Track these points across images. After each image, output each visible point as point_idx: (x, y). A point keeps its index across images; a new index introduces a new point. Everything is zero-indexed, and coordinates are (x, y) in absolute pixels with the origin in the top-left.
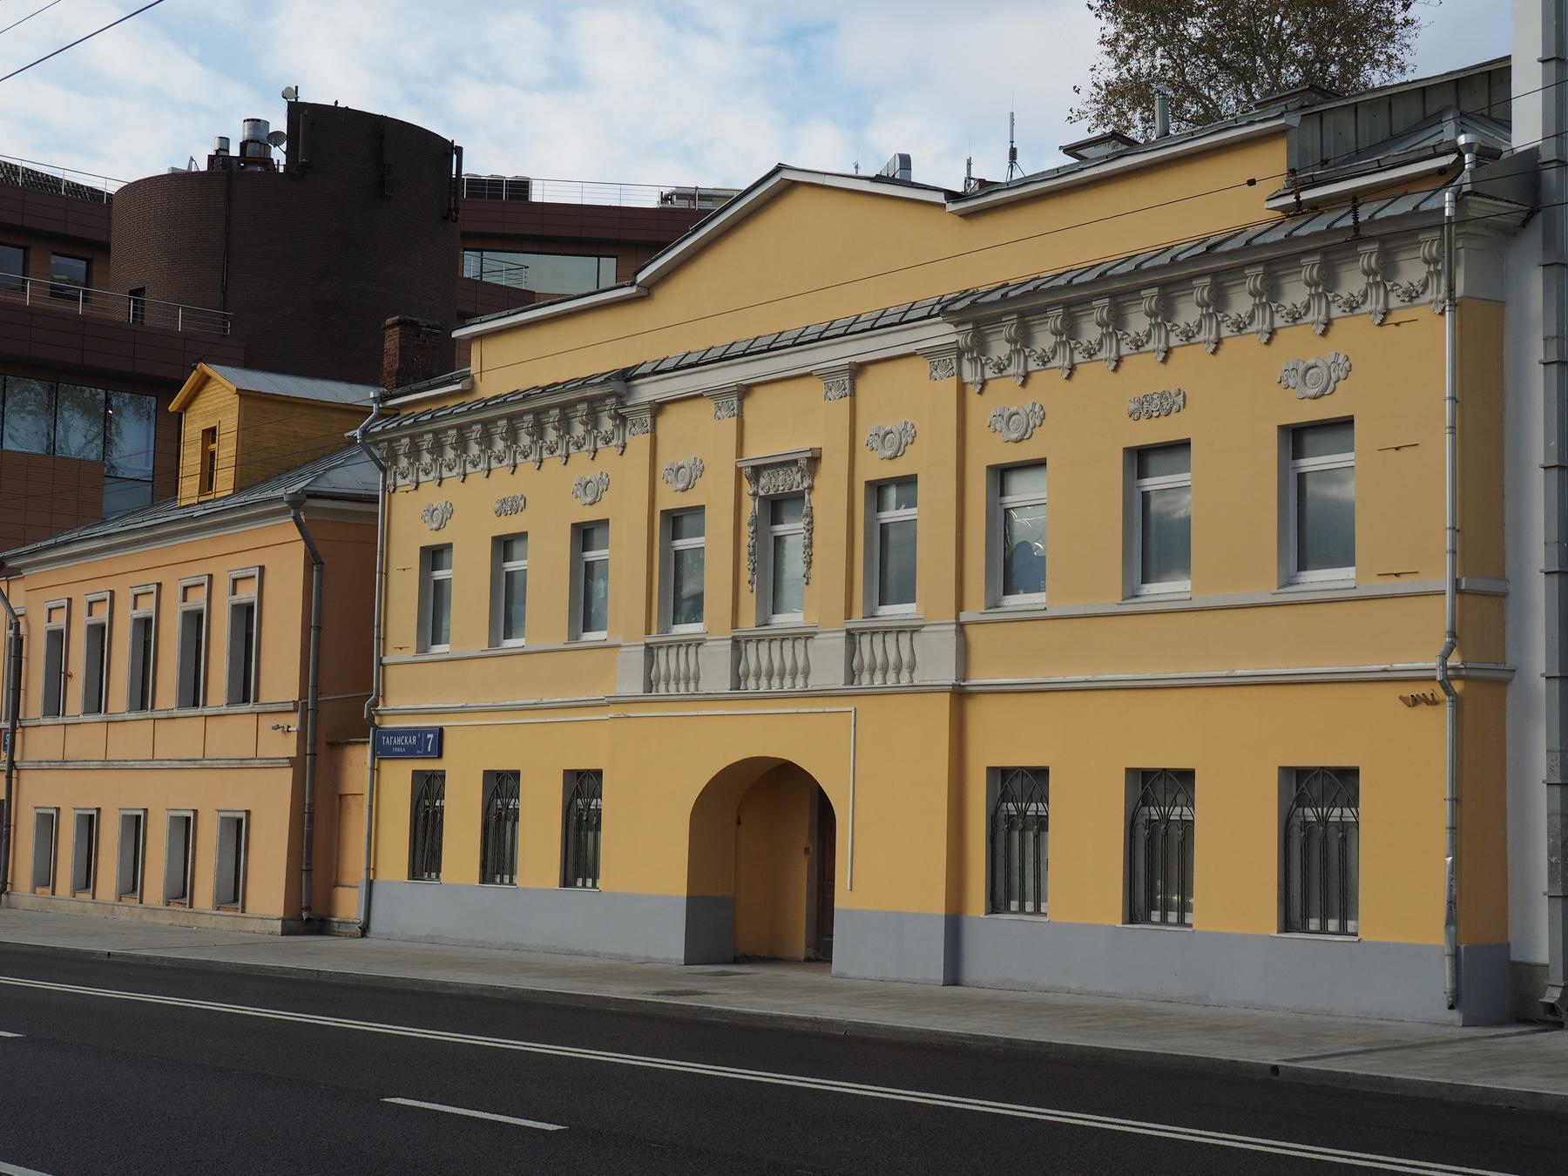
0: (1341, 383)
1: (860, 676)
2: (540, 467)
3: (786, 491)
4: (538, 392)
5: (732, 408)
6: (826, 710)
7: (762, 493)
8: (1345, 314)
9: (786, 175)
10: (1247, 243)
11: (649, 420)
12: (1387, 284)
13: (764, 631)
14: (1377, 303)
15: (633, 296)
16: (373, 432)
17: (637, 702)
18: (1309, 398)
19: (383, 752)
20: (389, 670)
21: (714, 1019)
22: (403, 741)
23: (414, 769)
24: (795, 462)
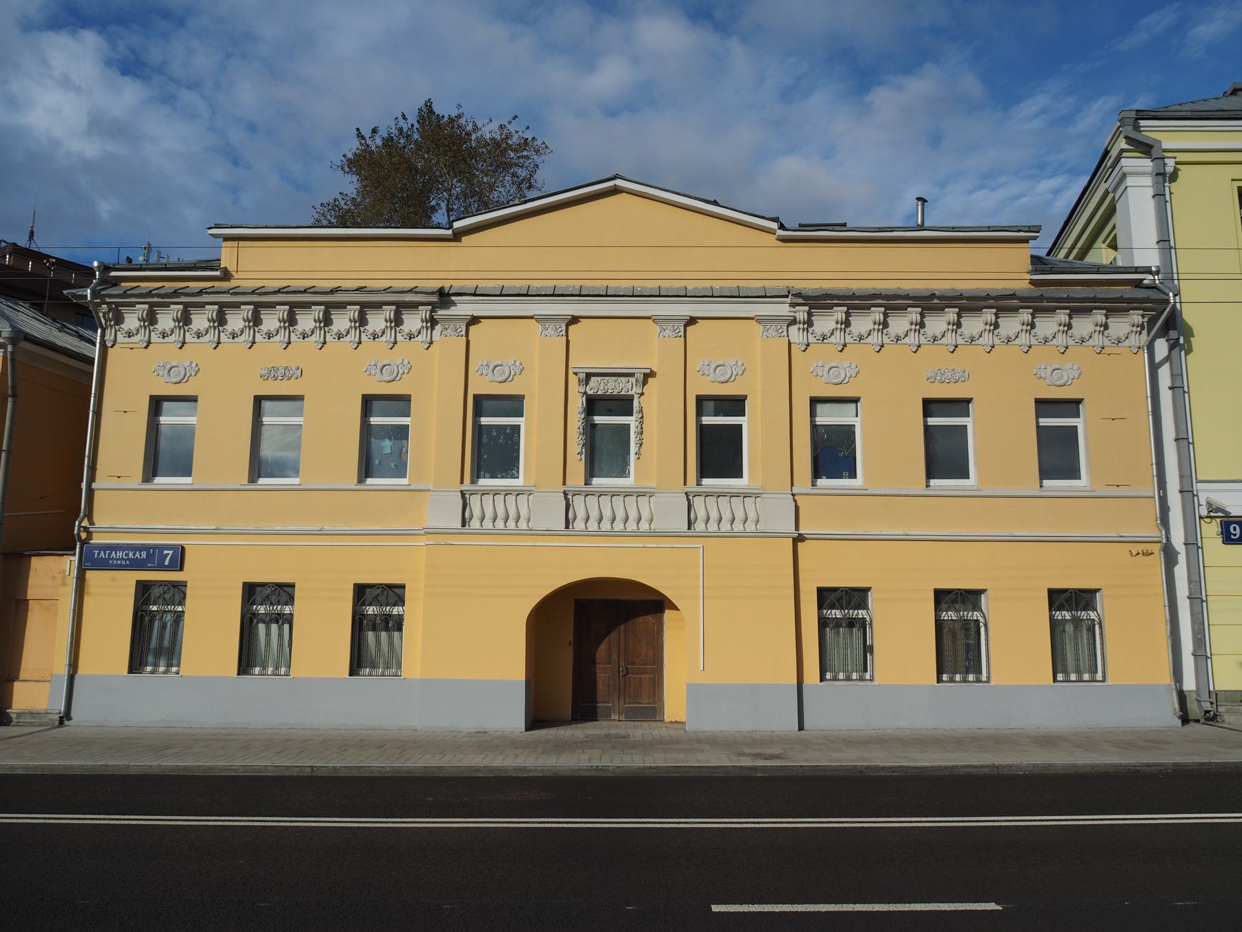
0: (1075, 381)
1: (469, 522)
2: (806, 349)
3: (614, 393)
4: (156, 292)
5: (780, 331)
6: (674, 546)
7: (590, 392)
8: (334, 340)
9: (619, 182)
10: (125, 292)
11: (564, 327)
12: (185, 327)
13: (588, 488)
14: (249, 337)
15: (448, 237)
16: (104, 294)
17: (438, 533)
18: (719, 382)
19: (93, 560)
20: (96, 493)
21: (881, 774)
22: (127, 555)
23: (819, 586)
24: (632, 375)
